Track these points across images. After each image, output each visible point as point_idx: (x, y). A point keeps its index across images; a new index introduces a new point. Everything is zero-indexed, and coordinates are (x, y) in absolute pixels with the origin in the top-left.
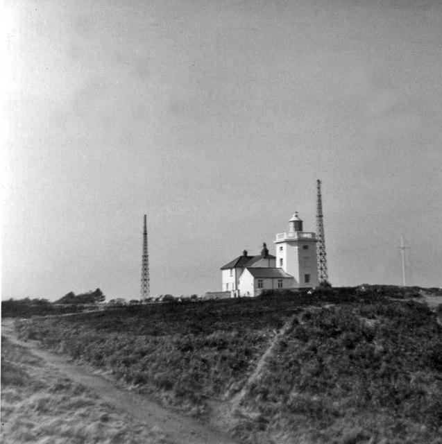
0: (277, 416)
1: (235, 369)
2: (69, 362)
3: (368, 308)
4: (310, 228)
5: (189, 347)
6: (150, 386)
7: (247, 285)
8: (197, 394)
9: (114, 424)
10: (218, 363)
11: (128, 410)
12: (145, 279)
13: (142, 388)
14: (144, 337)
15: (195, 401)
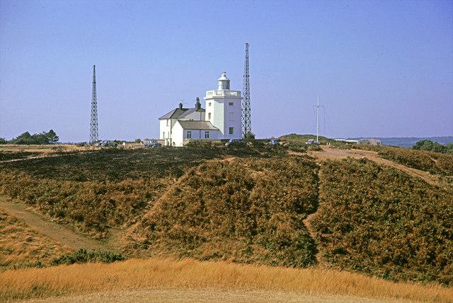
0: (158, 240)
1: (135, 207)
2: (8, 201)
3: (259, 161)
4: (237, 87)
5: (103, 191)
6: (67, 219)
7: (175, 136)
8: (102, 225)
9: (36, 243)
10: (122, 203)
11: (48, 235)
12: (94, 124)
13: (61, 220)
14: (68, 183)
15: (100, 230)
